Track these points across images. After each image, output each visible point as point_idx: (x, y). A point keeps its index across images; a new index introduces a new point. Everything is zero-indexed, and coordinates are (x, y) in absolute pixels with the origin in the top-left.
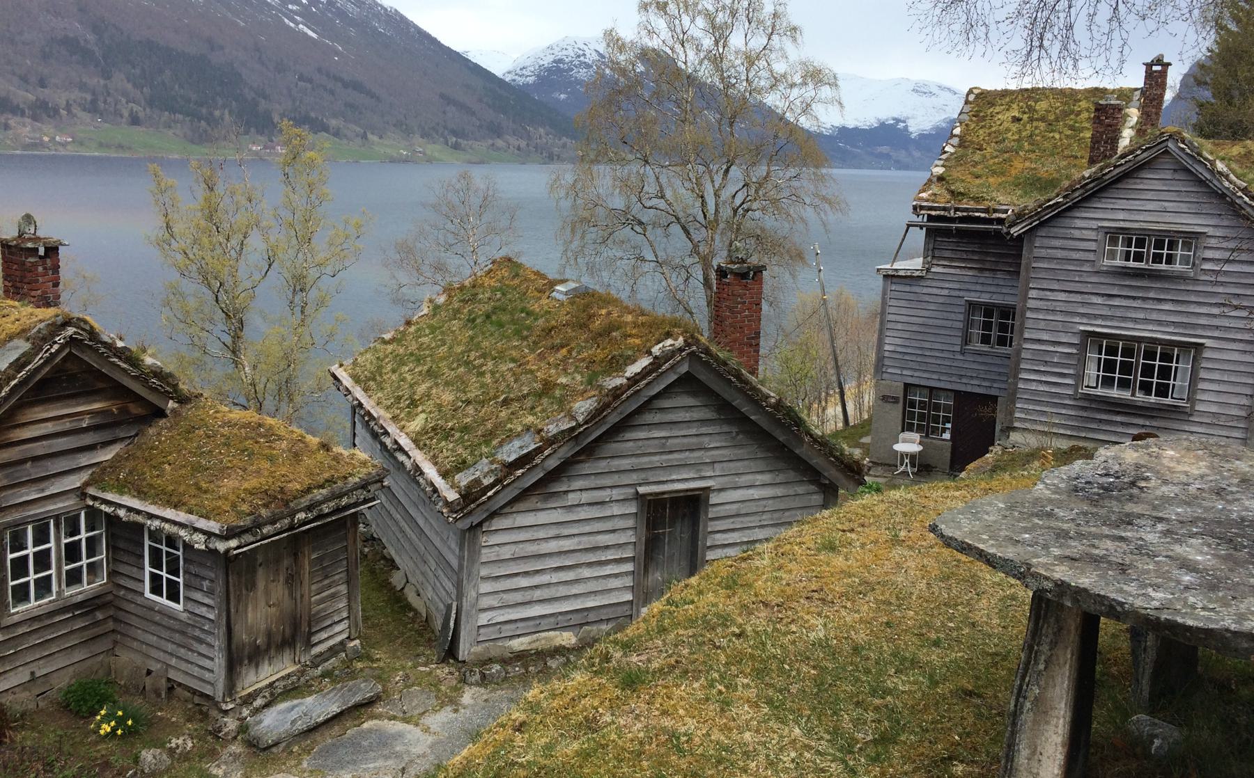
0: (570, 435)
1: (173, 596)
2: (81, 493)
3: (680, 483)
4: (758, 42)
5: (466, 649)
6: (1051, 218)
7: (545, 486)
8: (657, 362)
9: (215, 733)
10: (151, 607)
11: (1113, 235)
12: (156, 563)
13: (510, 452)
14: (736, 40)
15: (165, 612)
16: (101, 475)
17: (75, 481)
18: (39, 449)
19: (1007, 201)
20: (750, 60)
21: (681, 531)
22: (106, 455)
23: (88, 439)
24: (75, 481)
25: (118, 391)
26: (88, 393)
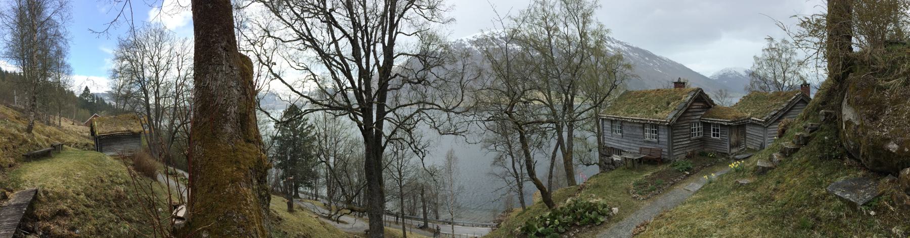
0: (783, 110)
1: (718, 135)
4: (788, 56)
14: (784, 56)
16: (702, 116)
20: (787, 60)
25: (705, 102)
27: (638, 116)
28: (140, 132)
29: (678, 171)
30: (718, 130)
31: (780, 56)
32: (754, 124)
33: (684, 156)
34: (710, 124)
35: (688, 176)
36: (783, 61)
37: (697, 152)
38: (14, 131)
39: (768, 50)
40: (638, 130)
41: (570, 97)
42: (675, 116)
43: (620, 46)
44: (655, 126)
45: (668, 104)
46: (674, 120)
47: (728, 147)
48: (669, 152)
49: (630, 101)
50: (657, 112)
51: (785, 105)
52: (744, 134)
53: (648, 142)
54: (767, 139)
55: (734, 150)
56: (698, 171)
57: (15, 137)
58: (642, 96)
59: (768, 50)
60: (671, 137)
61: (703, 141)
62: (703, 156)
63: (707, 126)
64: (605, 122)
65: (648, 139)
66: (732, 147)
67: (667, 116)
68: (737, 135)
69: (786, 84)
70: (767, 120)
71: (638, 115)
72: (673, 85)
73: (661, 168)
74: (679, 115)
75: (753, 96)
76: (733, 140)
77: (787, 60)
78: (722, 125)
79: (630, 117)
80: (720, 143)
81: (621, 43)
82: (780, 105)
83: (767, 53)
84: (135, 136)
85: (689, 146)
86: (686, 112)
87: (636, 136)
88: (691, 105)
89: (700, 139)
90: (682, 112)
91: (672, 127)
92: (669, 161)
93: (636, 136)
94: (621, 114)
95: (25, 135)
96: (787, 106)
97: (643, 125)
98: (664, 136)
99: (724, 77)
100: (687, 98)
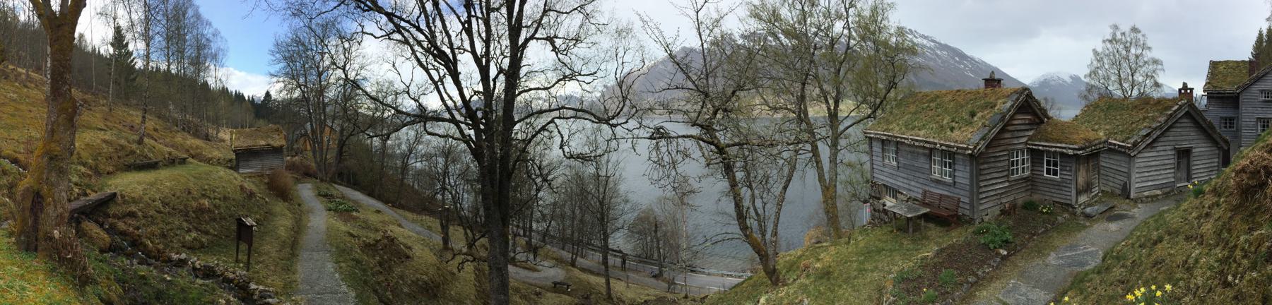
0: (1160, 127)
1: (1055, 174)
2: (1026, 143)
3: (1186, 145)
4: (1139, 51)
5: (1132, 195)
6: (1246, 88)
7: (1151, 146)
8: (1181, 107)
9: (1075, 214)
10: (1046, 179)
11: (1262, 92)
12: (1048, 164)
13: (1144, 132)
14: (1133, 51)
15: (1052, 180)
16: (1030, 138)
17: (1024, 140)
18: (1019, 127)
19: (1229, 88)
20: (1137, 57)
21: (1184, 161)
22: (1031, 133)
23: (1023, 127)
24: (1024, 140)
25: (1035, 114)
26: (1027, 113)
27: (921, 135)
28: (281, 147)
29: (985, 247)
30: (1055, 165)
31: (1128, 51)
32: (1112, 150)
33: (997, 211)
34: (1043, 152)
35: (1004, 258)
36: (1132, 58)
37: (1020, 202)
38: (123, 142)
39: (1110, 41)
40: (922, 159)
41: (408, 119)
42: (983, 139)
43: (925, 42)
44: (950, 155)
45: (973, 115)
46: (982, 146)
47: (1074, 192)
48: (971, 204)
49: (912, 108)
50: (952, 129)
51: (1162, 119)
52: (1098, 168)
53: (937, 182)
54: (1134, 176)
55: (1083, 199)
56: (1023, 246)
57: (123, 147)
58: (932, 101)
59: (1110, 41)
60: (977, 177)
61: (1031, 182)
62: (1032, 221)
63: (1036, 155)
64: (874, 144)
65: (937, 176)
66: (1079, 193)
67: (968, 136)
68: (1088, 171)
69: (1135, 93)
70: (1135, 145)
71: (922, 133)
72: (982, 84)
73: (957, 237)
74: (991, 136)
75: (1102, 104)
76: (1081, 180)
77: (1137, 57)
78: (1062, 154)
79: (909, 136)
80: (1058, 185)
81: (926, 38)
82: (1153, 119)
83: (1109, 45)
84: (277, 151)
85: (1007, 192)
86: (1003, 130)
87: (919, 170)
88: (1012, 118)
89: (1026, 179)
90: (996, 130)
91: (976, 159)
92: (971, 222)
93: (919, 170)
94: (896, 131)
95: (134, 146)
96: (1166, 121)
97: (931, 152)
98: (963, 175)
99: (1045, 83)
100: (1005, 105)
